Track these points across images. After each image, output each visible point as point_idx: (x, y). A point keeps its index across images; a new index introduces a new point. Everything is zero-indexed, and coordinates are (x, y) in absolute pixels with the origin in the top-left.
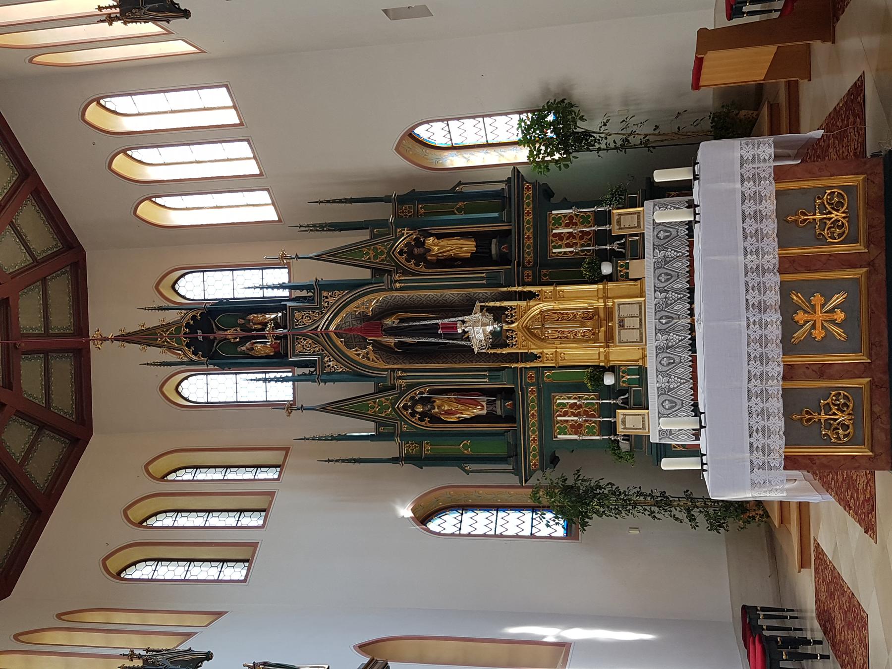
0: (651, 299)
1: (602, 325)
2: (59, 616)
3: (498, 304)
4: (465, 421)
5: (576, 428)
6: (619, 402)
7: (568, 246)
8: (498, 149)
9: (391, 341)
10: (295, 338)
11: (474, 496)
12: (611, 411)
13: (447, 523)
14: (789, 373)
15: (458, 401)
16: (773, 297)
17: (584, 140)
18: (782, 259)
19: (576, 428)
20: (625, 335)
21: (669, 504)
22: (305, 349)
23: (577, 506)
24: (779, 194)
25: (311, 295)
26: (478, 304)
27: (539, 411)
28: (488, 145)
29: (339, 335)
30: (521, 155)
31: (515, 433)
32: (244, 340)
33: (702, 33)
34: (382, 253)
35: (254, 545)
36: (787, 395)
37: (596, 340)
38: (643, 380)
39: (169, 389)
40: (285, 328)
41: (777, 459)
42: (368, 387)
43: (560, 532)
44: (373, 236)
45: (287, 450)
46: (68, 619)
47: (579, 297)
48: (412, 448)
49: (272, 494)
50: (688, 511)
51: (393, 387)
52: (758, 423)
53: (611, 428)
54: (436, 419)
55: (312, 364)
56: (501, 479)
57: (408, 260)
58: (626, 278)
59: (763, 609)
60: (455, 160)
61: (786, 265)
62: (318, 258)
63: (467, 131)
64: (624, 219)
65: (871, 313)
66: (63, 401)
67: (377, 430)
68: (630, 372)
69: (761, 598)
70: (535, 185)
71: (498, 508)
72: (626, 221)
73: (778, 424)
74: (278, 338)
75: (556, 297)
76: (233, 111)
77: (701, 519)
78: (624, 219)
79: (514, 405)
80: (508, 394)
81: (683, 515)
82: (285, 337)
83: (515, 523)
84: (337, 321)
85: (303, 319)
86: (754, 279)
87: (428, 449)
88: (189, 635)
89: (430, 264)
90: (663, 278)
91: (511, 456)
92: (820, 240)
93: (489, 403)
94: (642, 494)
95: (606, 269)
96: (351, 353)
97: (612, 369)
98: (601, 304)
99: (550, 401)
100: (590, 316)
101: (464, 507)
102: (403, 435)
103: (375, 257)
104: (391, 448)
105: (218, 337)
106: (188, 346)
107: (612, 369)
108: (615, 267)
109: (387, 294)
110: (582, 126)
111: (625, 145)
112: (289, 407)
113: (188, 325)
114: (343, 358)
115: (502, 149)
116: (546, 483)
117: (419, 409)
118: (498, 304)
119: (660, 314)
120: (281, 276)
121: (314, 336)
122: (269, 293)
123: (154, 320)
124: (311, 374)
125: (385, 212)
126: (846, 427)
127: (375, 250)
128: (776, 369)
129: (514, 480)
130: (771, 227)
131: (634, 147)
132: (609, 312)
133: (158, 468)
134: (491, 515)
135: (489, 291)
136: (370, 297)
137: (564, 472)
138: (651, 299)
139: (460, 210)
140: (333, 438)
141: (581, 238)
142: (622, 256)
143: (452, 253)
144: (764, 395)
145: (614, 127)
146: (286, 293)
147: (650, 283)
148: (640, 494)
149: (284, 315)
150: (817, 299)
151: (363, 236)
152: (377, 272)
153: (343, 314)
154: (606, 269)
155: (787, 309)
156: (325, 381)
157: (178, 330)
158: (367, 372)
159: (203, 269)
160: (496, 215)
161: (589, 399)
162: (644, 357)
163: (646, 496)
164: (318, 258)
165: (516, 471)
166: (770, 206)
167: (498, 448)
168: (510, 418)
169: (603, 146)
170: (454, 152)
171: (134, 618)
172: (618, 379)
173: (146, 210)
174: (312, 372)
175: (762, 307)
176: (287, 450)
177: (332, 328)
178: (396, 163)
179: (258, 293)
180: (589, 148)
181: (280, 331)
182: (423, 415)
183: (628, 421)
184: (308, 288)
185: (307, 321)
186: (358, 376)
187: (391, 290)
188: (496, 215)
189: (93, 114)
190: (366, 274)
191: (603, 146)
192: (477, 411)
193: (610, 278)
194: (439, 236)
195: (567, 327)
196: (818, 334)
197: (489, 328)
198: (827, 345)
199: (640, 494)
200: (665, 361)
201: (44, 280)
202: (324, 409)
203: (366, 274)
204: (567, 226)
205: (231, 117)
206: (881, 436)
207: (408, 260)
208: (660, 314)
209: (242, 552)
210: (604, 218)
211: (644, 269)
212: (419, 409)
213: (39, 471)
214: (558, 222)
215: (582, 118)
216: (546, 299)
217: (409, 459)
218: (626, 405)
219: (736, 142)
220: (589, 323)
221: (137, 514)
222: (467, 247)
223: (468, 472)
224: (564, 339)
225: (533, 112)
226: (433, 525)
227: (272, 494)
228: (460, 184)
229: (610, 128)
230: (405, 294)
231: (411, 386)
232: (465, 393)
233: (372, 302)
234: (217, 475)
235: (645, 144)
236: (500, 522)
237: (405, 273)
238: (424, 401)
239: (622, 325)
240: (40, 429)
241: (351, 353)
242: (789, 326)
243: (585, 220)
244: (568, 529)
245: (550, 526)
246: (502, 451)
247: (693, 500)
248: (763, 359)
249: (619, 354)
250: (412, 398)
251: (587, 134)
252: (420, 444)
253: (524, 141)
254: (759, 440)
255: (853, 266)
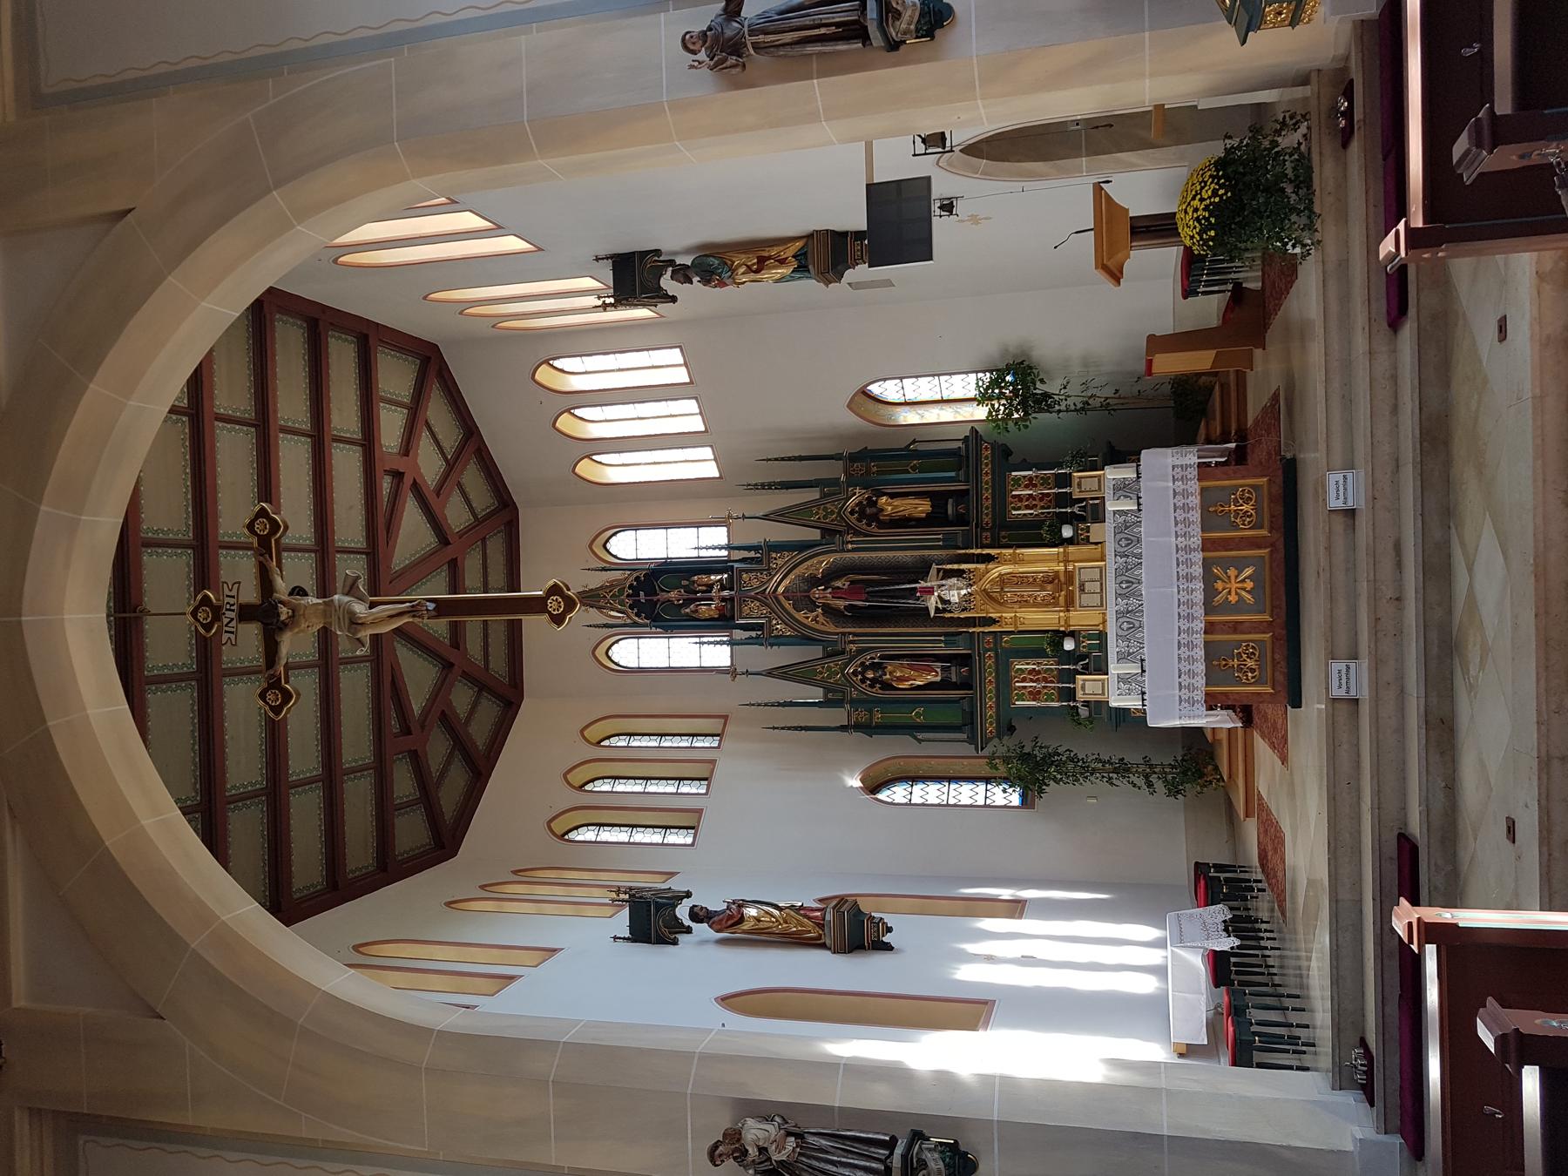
0: (1111, 563)
1: (1062, 588)
2: (483, 887)
3: (956, 566)
4: (919, 688)
5: (1035, 695)
6: (1079, 667)
7: (1027, 507)
8: (954, 406)
9: (841, 604)
10: (742, 601)
11: (924, 767)
12: (1070, 676)
13: (898, 793)
14: (1210, 628)
15: (911, 667)
16: (1198, 570)
17: (1045, 402)
18: (1204, 540)
19: (1035, 695)
20: (1086, 599)
21: (1128, 770)
22: (753, 612)
23: (1032, 774)
24: (1203, 490)
25: (761, 556)
26: (934, 566)
27: (997, 677)
28: (942, 401)
29: (788, 599)
30: (981, 412)
31: (972, 700)
32: (688, 602)
33: (1152, 339)
34: (832, 512)
35: (699, 812)
36: (1207, 645)
37: (1056, 604)
38: (1103, 647)
39: (600, 652)
40: (731, 589)
41: (1199, 695)
42: (816, 651)
43: (1015, 799)
44: (824, 496)
45: (726, 718)
46: (521, 874)
47: (1040, 560)
48: (863, 716)
49: (713, 762)
50: (1147, 777)
51: (843, 653)
52: (1185, 667)
53: (1070, 694)
54: (887, 686)
55: (760, 627)
56: (954, 748)
57: (859, 520)
58: (1087, 541)
59: (1215, 866)
60: (909, 417)
61: (1207, 545)
62: (766, 517)
63: (922, 388)
64: (1084, 482)
65: (1273, 583)
66: (498, 664)
67: (825, 695)
68: (1090, 637)
69: (1216, 854)
70: (994, 445)
71: (951, 779)
72: (1086, 485)
73: (1200, 667)
74: (723, 599)
75: (1015, 560)
76: (684, 369)
77: (1159, 785)
78: (1084, 482)
79: (971, 671)
80: (964, 660)
81: (1140, 781)
82: (731, 599)
83: (967, 793)
84: (786, 582)
85: (751, 581)
86: (1183, 556)
87: (878, 717)
88: (672, 874)
89: (882, 524)
90: (1123, 543)
91: (968, 725)
92: (1235, 527)
93: (943, 669)
94: (1100, 761)
95: (1067, 532)
96: (800, 616)
97: (1072, 634)
98: (1061, 568)
99: (1008, 666)
100: (1051, 579)
101: (914, 779)
102: (852, 702)
103: (825, 517)
104: (839, 716)
105: (659, 597)
106: (631, 607)
107: (1072, 634)
108: (1075, 531)
109: (838, 556)
110: (1041, 388)
111: (1085, 408)
112: (732, 672)
113: (631, 587)
114: (790, 621)
115: (958, 405)
116: (1002, 751)
117: (870, 675)
118: (956, 566)
119: (1120, 579)
120: (719, 535)
121: (761, 597)
122: (704, 553)
123: (596, 580)
124: (758, 637)
125: (836, 470)
126: (1252, 671)
127: (825, 509)
128: (1199, 625)
129: (969, 749)
130: (1196, 516)
131: (1094, 409)
132: (1070, 576)
133: (594, 733)
134: (944, 787)
135: (944, 553)
136: (821, 558)
137: (1024, 737)
138: (1111, 563)
139: (914, 468)
140: (779, 705)
141: (1041, 500)
142: (1082, 519)
143: (906, 513)
144: (1190, 646)
145: (1074, 389)
146: (724, 553)
147: (1110, 548)
148: (1098, 760)
149: (731, 578)
150: (1232, 572)
151: (813, 494)
152: (827, 533)
153: (792, 576)
154: (1067, 532)
155: (1209, 579)
156: (772, 645)
157: (621, 591)
158: (816, 635)
159: (636, 528)
160: (953, 474)
161: (1049, 664)
162: (1104, 622)
163: (1104, 763)
164: (766, 517)
165: (972, 740)
166: (1195, 501)
167: (952, 716)
168: (966, 685)
169: (1063, 407)
170: (907, 408)
171: (586, 875)
172: (1077, 644)
173: (585, 469)
174: (763, 635)
175: (1189, 578)
176: (726, 718)
177: (781, 589)
178: (850, 420)
179: (694, 554)
180: (1049, 409)
181: (726, 593)
182: (874, 681)
183: (1088, 686)
184: (755, 548)
185: (755, 583)
186: (806, 640)
187: (843, 551)
188: (953, 474)
189: (544, 374)
190: (815, 535)
191: (1063, 407)
192: (931, 678)
193: (1070, 541)
194: (893, 496)
195: (1026, 591)
196: (1233, 598)
197: (963, 592)
198: (1240, 606)
199: (1098, 760)
200: (1125, 626)
201: (484, 540)
202: (770, 673)
203: (815, 535)
204: (1027, 487)
205: (681, 376)
206: (1280, 678)
207: (859, 520)
208: (1120, 579)
209: (689, 820)
210: (1065, 481)
211: (1104, 532)
212: (870, 675)
213: (479, 732)
214: (1017, 481)
215: (1042, 381)
216: (1006, 562)
217: (858, 727)
218: (1086, 670)
219: (1169, 451)
220: (1049, 587)
221: (577, 777)
222: (923, 507)
223: (920, 741)
224: (1024, 603)
225: (991, 372)
226: (883, 795)
227: (713, 762)
228: (914, 442)
229: (1069, 391)
230: (856, 555)
231: (860, 651)
232: (920, 659)
233: (823, 563)
234: (653, 742)
235: (1106, 406)
236: (952, 793)
237: (857, 533)
238: (874, 667)
239: (1082, 590)
240: (480, 690)
241: (800, 616)
242: (1210, 592)
243: (1045, 481)
244: (1023, 797)
245: (1005, 796)
246: (957, 720)
247: (1151, 766)
248: (1190, 618)
249: (1080, 618)
250: (862, 664)
251: (1047, 395)
252: (870, 711)
253: (983, 398)
254: (1186, 680)
255: (1259, 547)
